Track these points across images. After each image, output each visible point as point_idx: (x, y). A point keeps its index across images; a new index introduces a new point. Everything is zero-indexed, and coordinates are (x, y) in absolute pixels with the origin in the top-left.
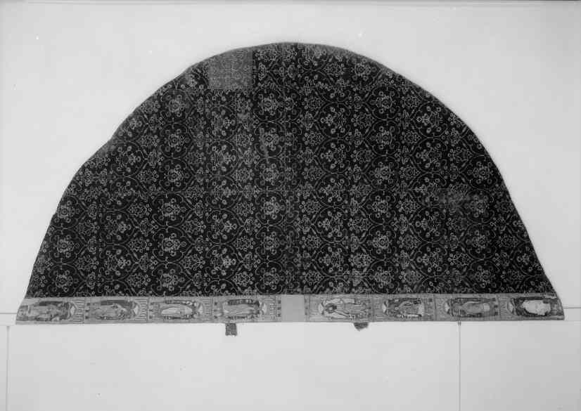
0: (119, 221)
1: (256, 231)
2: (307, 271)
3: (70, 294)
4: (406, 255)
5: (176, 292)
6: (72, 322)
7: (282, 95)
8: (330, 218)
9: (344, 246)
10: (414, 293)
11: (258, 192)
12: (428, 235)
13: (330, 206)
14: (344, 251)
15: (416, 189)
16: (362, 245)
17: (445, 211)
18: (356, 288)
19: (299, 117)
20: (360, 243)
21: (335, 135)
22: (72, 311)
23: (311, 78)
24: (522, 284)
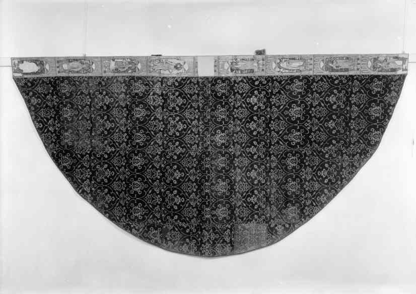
3: (372, 78)
5: (292, 79)
15: (114, 150)
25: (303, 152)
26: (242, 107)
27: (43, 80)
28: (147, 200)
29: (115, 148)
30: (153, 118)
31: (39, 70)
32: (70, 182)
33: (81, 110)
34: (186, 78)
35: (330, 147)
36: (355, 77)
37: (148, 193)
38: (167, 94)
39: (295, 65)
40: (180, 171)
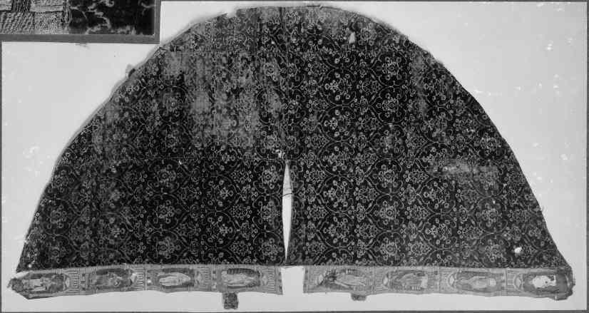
0: (112, 226)
1: (253, 199)
2: (310, 242)
3: (63, 264)
4: (414, 226)
5: (173, 259)
6: (67, 294)
7: (285, 61)
8: (335, 188)
9: (350, 216)
10: (419, 265)
11: (258, 159)
12: (437, 207)
13: (335, 176)
14: (350, 221)
15: (423, 159)
16: (368, 251)
17: (454, 182)
18: (360, 260)
19: (303, 84)
20: (367, 249)
21: (339, 102)
22: (67, 283)
23: (316, 42)
24: (534, 259)
25: (156, 154)
26: (239, 220)
27: (526, 264)
28: (377, 85)
29: (422, 161)
30: (370, 205)
31: (532, 279)
32: (485, 114)
33: (472, 218)
34: (319, 264)
35: (120, 162)
36: (87, 263)
37: (377, 95)
38: (350, 240)
39: (169, 280)
40: (330, 129)
